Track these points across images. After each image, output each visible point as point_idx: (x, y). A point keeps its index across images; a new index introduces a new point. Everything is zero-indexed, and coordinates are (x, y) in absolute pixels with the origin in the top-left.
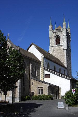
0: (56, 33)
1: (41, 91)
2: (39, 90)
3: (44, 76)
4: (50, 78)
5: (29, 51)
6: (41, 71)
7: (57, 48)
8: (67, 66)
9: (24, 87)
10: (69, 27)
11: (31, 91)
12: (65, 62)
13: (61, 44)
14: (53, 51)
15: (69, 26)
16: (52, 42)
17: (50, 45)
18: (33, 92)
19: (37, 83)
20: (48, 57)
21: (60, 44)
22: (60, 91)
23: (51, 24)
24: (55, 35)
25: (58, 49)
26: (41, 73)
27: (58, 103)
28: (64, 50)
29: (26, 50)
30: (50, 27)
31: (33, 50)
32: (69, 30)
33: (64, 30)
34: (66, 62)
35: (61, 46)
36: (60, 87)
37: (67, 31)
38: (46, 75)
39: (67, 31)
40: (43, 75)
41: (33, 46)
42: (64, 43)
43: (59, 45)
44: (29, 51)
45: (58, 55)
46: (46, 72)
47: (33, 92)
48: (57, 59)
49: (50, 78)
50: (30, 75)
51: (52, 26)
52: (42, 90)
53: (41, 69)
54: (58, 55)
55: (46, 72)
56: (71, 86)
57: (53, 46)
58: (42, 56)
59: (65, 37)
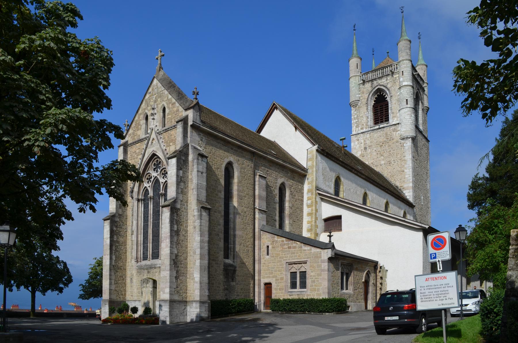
0: (375, 82)
1: (298, 279)
2: (293, 275)
3: (321, 225)
5: (264, 133)
6: (308, 206)
7: (379, 136)
9: (228, 261)
10: (421, 61)
11: (264, 280)
12: (405, 186)
13: (392, 121)
14: (365, 148)
15: (421, 57)
16: (363, 116)
17: (354, 128)
18: (270, 284)
19: (282, 245)
20: (334, 153)
21: (387, 120)
22: (381, 278)
23: (355, 52)
24: (370, 89)
25: (382, 139)
26: (309, 214)
27: (129, 181)
28: (403, 139)
29: (254, 130)
30: (354, 62)
31: (281, 132)
32: (421, 71)
33: (405, 67)
34: (411, 185)
35: (393, 127)
36: (381, 263)
37: (414, 68)
38: (326, 220)
40: (316, 219)
41: (277, 116)
42: (402, 116)
43: (385, 125)
44: (264, 133)
45: (383, 162)
46: (328, 210)
47: (270, 284)
48: (379, 175)
49: (340, 230)
50: (257, 216)
51: (361, 59)
52: (303, 274)
53: (309, 199)
54: (383, 162)
55: (328, 210)
56: (397, 193)
57: (364, 130)
59: (407, 93)
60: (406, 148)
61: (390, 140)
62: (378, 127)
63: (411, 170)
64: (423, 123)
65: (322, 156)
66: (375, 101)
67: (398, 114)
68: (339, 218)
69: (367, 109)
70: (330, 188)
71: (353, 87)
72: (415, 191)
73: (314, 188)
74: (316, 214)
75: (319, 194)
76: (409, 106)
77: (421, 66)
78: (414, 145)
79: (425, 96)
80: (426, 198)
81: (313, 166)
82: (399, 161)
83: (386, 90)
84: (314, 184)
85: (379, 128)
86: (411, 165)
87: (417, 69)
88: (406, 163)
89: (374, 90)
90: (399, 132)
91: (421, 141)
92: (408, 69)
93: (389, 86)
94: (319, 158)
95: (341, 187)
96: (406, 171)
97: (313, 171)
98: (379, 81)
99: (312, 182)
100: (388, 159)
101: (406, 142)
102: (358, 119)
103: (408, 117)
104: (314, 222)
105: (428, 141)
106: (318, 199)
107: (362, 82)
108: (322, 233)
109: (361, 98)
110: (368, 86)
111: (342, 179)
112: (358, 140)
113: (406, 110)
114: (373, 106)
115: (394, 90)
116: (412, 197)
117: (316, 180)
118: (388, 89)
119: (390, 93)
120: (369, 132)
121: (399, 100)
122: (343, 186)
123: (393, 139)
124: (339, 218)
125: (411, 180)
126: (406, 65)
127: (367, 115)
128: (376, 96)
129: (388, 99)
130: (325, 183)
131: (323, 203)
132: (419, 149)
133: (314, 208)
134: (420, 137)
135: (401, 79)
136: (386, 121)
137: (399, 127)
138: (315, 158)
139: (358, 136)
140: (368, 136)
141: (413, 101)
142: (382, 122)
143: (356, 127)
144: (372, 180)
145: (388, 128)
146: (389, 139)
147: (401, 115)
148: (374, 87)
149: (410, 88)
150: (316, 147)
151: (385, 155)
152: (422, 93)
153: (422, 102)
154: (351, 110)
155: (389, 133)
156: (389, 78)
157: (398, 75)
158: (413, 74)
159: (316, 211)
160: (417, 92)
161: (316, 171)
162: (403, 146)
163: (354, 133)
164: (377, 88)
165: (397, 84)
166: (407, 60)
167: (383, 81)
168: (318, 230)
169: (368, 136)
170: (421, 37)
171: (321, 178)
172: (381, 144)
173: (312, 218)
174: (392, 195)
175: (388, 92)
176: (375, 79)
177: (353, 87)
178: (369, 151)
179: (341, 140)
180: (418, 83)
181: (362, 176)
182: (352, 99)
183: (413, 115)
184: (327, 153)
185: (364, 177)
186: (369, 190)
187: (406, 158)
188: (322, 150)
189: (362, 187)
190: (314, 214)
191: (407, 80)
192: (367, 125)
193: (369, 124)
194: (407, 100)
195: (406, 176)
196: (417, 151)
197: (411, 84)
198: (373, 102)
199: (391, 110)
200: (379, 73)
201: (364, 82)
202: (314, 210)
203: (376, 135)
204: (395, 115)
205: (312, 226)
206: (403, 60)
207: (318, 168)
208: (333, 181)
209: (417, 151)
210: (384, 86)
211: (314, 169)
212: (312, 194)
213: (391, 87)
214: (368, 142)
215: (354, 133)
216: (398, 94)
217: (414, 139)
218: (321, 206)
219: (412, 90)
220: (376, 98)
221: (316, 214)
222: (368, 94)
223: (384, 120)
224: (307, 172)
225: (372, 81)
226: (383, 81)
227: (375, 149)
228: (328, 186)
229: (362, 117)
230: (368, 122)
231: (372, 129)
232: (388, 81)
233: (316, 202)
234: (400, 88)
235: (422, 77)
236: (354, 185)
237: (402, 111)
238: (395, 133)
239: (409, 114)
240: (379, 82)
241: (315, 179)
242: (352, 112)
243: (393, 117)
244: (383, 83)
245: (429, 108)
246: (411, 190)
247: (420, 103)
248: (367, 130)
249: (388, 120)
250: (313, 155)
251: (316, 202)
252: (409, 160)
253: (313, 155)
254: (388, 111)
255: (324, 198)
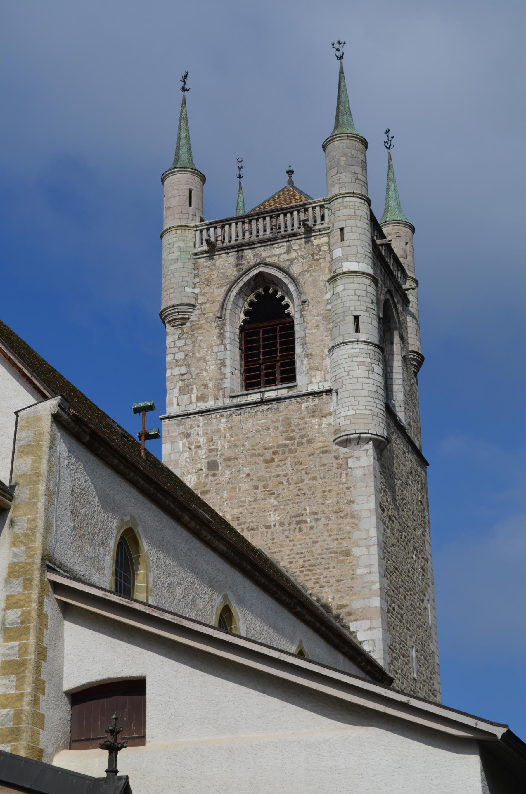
0: (249, 254)
3: (57, 714)
4: (143, 744)
7: (261, 426)
8: (391, 648)
12: (356, 605)
13: (306, 381)
14: (213, 466)
16: (203, 359)
21: (289, 376)
24: (233, 273)
28: (345, 443)
34: (376, 602)
35: (310, 402)
37: (376, 227)
38: (79, 697)
39: (426, 473)
40: (39, 687)
42: (339, 366)
43: (284, 393)
46: (90, 656)
49: (143, 744)
54: (274, 518)
57: (210, 404)
58: (30, 399)
59: (357, 296)
60: (358, 473)
61: (300, 444)
62: (256, 397)
63: (375, 550)
64: (406, 403)
65: (74, 443)
66: (246, 313)
67: (327, 361)
68: (135, 687)
69: (221, 336)
70: (100, 570)
71: (175, 261)
72: (389, 628)
73: (38, 560)
74: (38, 669)
75: (57, 587)
76: (362, 336)
77: (397, 228)
78: (382, 466)
79: (409, 319)
80: (425, 656)
81: (38, 475)
82: (332, 516)
83: (286, 280)
84: (38, 545)
85: (263, 402)
86: (373, 532)
87: (385, 230)
88: (355, 526)
89: (246, 279)
90: (331, 419)
91: (405, 463)
92: (359, 224)
93: (295, 269)
94: (63, 448)
95: (141, 572)
96: (356, 551)
97: (34, 495)
98: (265, 253)
99: (29, 536)
100: (296, 509)
101: (356, 453)
102: (188, 366)
103: (361, 372)
104: (27, 699)
105: (423, 462)
106: (51, 609)
107: (205, 247)
108: (58, 749)
109: (201, 299)
110: (226, 262)
111: (145, 546)
112: (187, 436)
113: (357, 349)
114: (242, 329)
115: (315, 283)
116: (380, 646)
117: (47, 529)
118: (294, 280)
119: (300, 293)
120: (227, 413)
121: (330, 318)
122: (147, 568)
123: (310, 442)
124: (135, 687)
125: (377, 586)
126: (352, 212)
127: (221, 356)
128: (252, 297)
129: (293, 310)
130: (80, 548)
131: (67, 624)
132: (398, 483)
133: (32, 641)
134: (398, 445)
135: (338, 253)
136: (284, 380)
137: (330, 404)
138: (46, 445)
139: (188, 422)
140: (223, 424)
141: (375, 323)
142: (271, 382)
143: (182, 391)
144: (251, 563)
145: (293, 405)
146: (296, 440)
147: (336, 365)
148: (245, 267)
149: (368, 281)
150: (52, 405)
151: (285, 492)
152: (400, 308)
153: (402, 337)
154: (165, 334)
155: (295, 420)
156: (296, 244)
157: (325, 240)
158: (373, 241)
159: (42, 653)
160: (386, 301)
161: (50, 495)
162: (344, 466)
163: (172, 409)
164: (255, 272)
165: (325, 264)
166: (354, 195)
167: (276, 251)
168: (43, 734)
169: (222, 426)
170: (393, 142)
171: (65, 526)
172: (269, 454)
173: (21, 681)
174: (317, 631)
175: (291, 287)
176: (251, 245)
177: (175, 261)
178: (225, 474)
179: (137, 410)
180: (389, 273)
181: (217, 543)
182: (170, 297)
183: (378, 369)
184: (93, 434)
185: (222, 547)
186: (241, 602)
187: (355, 508)
188: (76, 419)
189: (211, 584)
190: (31, 667)
191: (355, 257)
192: (219, 388)
193: (227, 384)
194: (357, 318)
195: (359, 571)
196: (392, 488)
197: (371, 271)
198: (242, 317)
199: (304, 344)
200: (264, 227)
201: (212, 250)
202: (32, 649)
203: (252, 422)
204: (315, 363)
205: (18, 716)
206: (343, 196)
207: (58, 486)
208: (112, 543)
209: (392, 488)
210: (279, 268)
211: (42, 487)
212: (27, 584)
213: (302, 273)
214: (222, 445)
215: (172, 409)
216: (328, 296)
217: (381, 446)
218: (59, 637)
219: (372, 290)
220: (251, 304)
221: (38, 669)
222: (224, 290)
223: (278, 376)
224: (11, 497)
225: (240, 247)
226: (277, 253)
227: (247, 470)
228: (92, 560)
229: (203, 359)
230: (223, 377)
231: (236, 401)
232: (293, 255)
233: (42, 617)
234: (333, 279)
235: (401, 260)
236: (187, 576)
237: (341, 352)
238: (316, 421)
239: (363, 364)
240: (264, 254)
241: (41, 524)
242: (169, 340)
243: (310, 368)
244: (275, 260)
245: (423, 358)
246: (378, 622)
247: (397, 339)
248: (220, 403)
249: (293, 379)
250: (39, 435)
251: (42, 617)
252: (365, 514)
253: (39, 435)
254: (293, 349)
255: (78, 605)
